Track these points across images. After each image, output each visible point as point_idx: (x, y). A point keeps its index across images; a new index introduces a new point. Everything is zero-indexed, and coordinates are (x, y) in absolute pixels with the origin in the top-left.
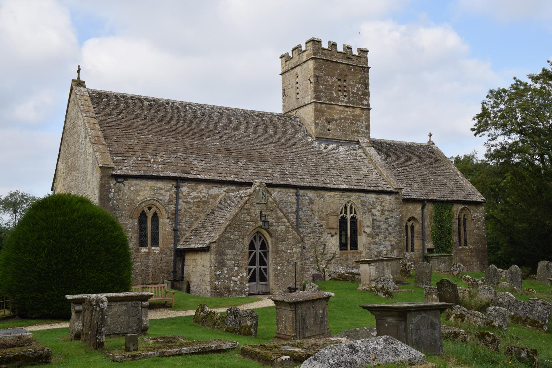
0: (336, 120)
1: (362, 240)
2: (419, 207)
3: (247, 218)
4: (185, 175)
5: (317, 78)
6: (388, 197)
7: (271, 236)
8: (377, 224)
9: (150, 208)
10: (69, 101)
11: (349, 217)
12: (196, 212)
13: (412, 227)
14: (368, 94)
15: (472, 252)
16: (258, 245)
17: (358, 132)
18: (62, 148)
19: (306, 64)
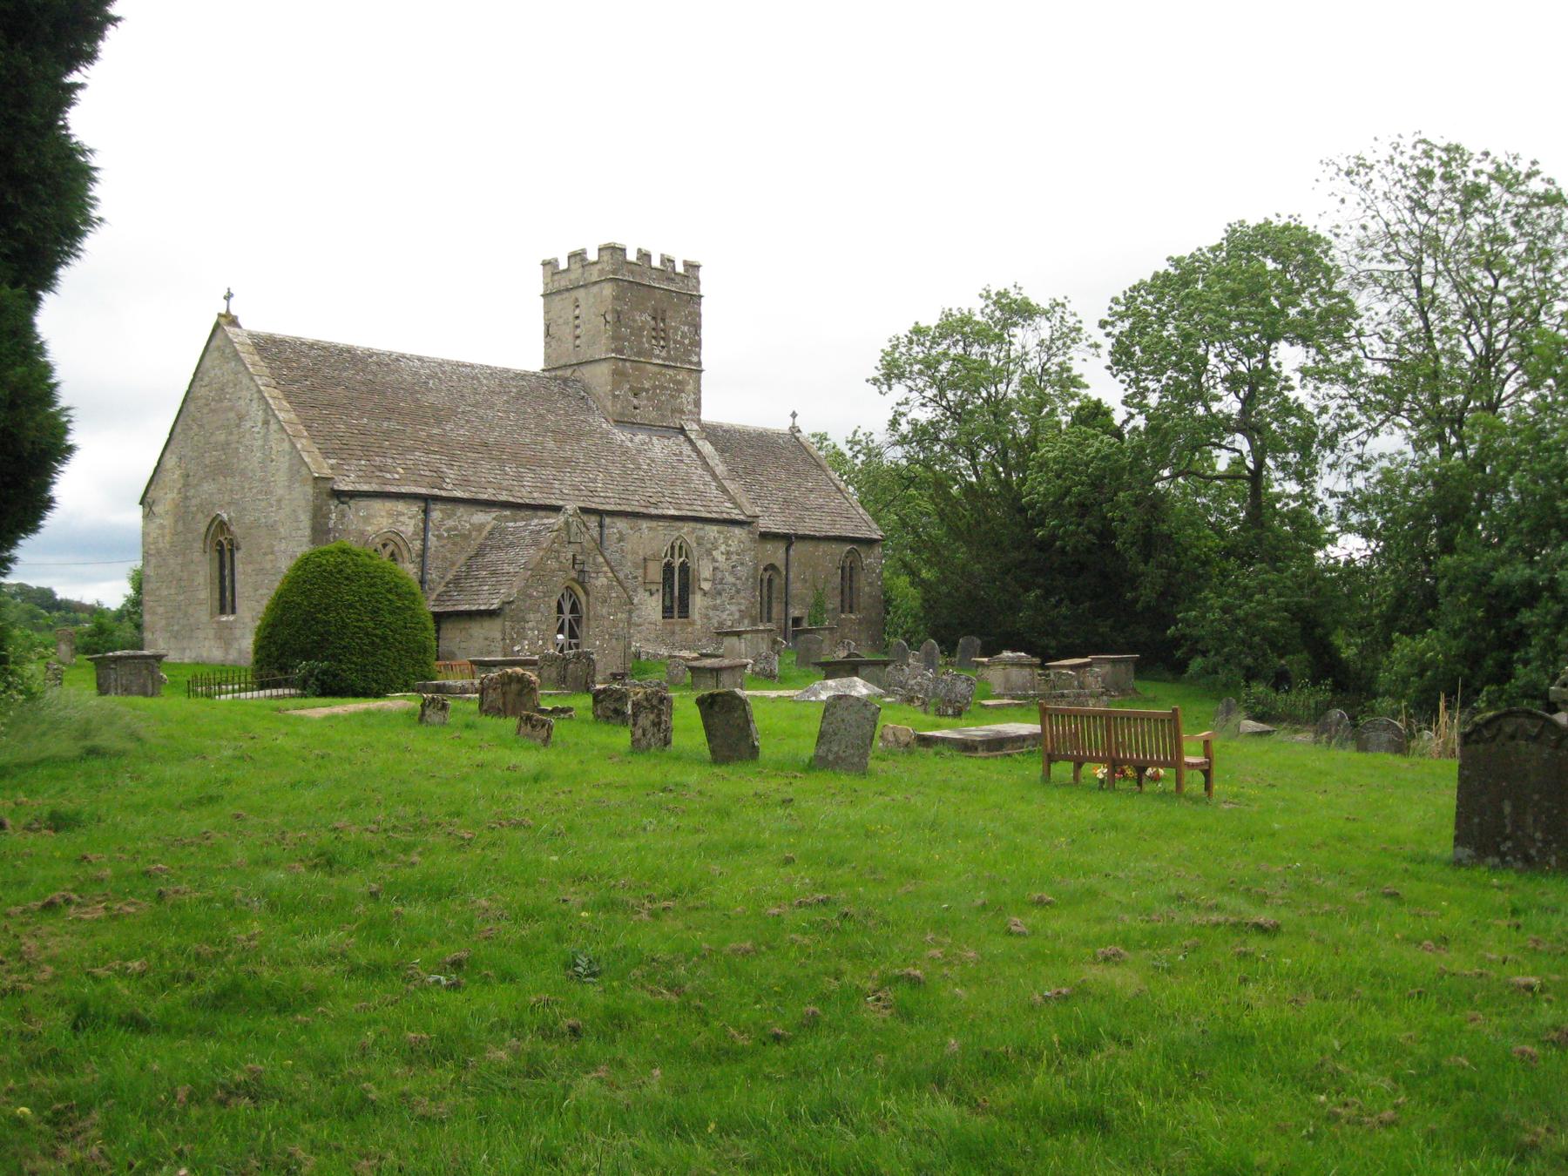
0: (647, 391)
1: (698, 602)
2: (780, 548)
3: (555, 565)
4: (436, 492)
5: (618, 315)
6: (737, 531)
7: (587, 593)
8: (719, 575)
9: (385, 546)
10: (206, 348)
11: (677, 562)
12: (451, 552)
13: (770, 581)
14: (698, 344)
15: (860, 623)
16: (567, 607)
17: (682, 412)
18: (178, 429)
19: (595, 289)
